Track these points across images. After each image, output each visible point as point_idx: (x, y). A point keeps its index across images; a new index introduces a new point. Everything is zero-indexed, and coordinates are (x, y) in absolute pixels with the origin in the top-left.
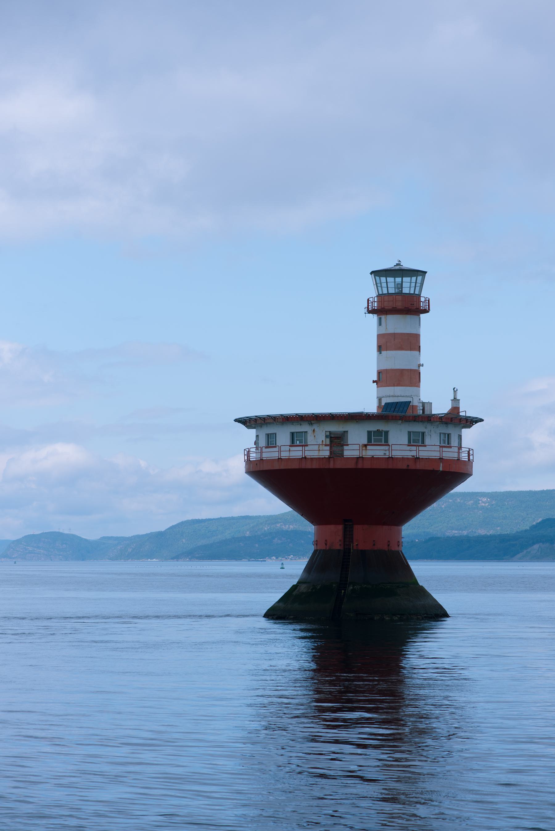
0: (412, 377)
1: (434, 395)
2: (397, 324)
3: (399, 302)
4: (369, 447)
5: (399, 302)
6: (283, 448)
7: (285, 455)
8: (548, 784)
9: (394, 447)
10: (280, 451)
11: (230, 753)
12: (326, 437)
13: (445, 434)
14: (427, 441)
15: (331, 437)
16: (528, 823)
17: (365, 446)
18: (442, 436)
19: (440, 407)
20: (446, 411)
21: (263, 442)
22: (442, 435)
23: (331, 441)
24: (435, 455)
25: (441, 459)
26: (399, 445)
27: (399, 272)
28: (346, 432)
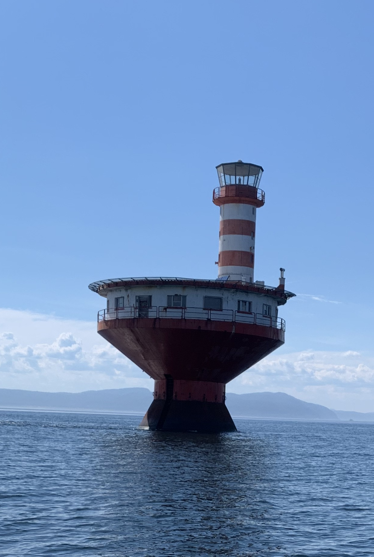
0: (247, 259)
1: (265, 274)
2: (237, 211)
3: (241, 195)
4: (168, 310)
5: (241, 195)
6: (258, 316)
7: (258, 322)
8: (329, 535)
9: (188, 310)
10: (255, 318)
11: (8, 538)
12: (137, 301)
13: (245, 302)
14: (224, 306)
15: (140, 302)
16: (42, 505)
17: (165, 309)
18: (265, 307)
19: (272, 283)
20: (276, 287)
21: (113, 305)
22: (241, 303)
23: (140, 305)
24: (229, 319)
25: (234, 323)
26: (229, 310)
27: (239, 168)
28: (150, 297)
